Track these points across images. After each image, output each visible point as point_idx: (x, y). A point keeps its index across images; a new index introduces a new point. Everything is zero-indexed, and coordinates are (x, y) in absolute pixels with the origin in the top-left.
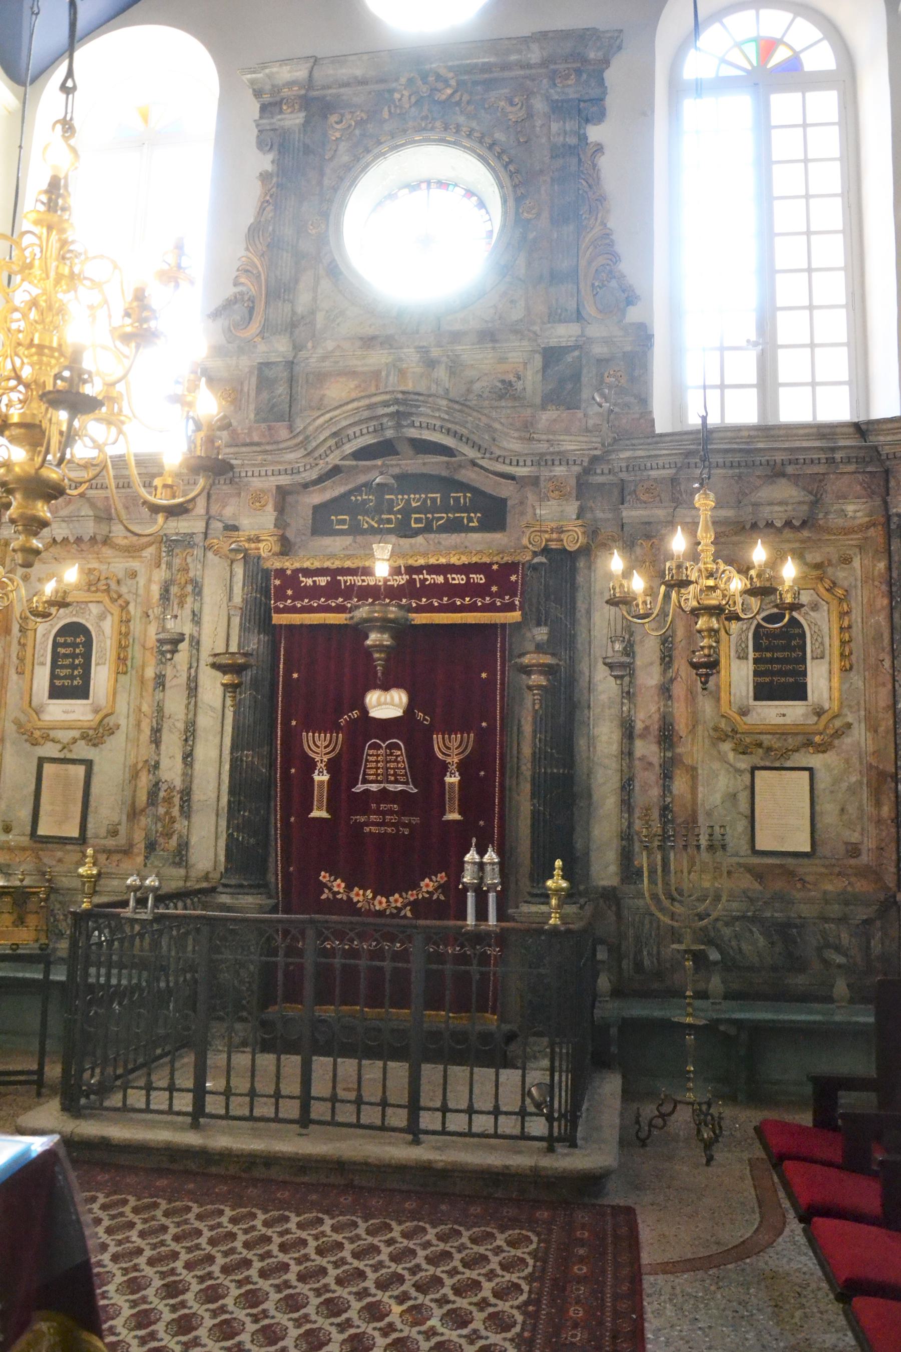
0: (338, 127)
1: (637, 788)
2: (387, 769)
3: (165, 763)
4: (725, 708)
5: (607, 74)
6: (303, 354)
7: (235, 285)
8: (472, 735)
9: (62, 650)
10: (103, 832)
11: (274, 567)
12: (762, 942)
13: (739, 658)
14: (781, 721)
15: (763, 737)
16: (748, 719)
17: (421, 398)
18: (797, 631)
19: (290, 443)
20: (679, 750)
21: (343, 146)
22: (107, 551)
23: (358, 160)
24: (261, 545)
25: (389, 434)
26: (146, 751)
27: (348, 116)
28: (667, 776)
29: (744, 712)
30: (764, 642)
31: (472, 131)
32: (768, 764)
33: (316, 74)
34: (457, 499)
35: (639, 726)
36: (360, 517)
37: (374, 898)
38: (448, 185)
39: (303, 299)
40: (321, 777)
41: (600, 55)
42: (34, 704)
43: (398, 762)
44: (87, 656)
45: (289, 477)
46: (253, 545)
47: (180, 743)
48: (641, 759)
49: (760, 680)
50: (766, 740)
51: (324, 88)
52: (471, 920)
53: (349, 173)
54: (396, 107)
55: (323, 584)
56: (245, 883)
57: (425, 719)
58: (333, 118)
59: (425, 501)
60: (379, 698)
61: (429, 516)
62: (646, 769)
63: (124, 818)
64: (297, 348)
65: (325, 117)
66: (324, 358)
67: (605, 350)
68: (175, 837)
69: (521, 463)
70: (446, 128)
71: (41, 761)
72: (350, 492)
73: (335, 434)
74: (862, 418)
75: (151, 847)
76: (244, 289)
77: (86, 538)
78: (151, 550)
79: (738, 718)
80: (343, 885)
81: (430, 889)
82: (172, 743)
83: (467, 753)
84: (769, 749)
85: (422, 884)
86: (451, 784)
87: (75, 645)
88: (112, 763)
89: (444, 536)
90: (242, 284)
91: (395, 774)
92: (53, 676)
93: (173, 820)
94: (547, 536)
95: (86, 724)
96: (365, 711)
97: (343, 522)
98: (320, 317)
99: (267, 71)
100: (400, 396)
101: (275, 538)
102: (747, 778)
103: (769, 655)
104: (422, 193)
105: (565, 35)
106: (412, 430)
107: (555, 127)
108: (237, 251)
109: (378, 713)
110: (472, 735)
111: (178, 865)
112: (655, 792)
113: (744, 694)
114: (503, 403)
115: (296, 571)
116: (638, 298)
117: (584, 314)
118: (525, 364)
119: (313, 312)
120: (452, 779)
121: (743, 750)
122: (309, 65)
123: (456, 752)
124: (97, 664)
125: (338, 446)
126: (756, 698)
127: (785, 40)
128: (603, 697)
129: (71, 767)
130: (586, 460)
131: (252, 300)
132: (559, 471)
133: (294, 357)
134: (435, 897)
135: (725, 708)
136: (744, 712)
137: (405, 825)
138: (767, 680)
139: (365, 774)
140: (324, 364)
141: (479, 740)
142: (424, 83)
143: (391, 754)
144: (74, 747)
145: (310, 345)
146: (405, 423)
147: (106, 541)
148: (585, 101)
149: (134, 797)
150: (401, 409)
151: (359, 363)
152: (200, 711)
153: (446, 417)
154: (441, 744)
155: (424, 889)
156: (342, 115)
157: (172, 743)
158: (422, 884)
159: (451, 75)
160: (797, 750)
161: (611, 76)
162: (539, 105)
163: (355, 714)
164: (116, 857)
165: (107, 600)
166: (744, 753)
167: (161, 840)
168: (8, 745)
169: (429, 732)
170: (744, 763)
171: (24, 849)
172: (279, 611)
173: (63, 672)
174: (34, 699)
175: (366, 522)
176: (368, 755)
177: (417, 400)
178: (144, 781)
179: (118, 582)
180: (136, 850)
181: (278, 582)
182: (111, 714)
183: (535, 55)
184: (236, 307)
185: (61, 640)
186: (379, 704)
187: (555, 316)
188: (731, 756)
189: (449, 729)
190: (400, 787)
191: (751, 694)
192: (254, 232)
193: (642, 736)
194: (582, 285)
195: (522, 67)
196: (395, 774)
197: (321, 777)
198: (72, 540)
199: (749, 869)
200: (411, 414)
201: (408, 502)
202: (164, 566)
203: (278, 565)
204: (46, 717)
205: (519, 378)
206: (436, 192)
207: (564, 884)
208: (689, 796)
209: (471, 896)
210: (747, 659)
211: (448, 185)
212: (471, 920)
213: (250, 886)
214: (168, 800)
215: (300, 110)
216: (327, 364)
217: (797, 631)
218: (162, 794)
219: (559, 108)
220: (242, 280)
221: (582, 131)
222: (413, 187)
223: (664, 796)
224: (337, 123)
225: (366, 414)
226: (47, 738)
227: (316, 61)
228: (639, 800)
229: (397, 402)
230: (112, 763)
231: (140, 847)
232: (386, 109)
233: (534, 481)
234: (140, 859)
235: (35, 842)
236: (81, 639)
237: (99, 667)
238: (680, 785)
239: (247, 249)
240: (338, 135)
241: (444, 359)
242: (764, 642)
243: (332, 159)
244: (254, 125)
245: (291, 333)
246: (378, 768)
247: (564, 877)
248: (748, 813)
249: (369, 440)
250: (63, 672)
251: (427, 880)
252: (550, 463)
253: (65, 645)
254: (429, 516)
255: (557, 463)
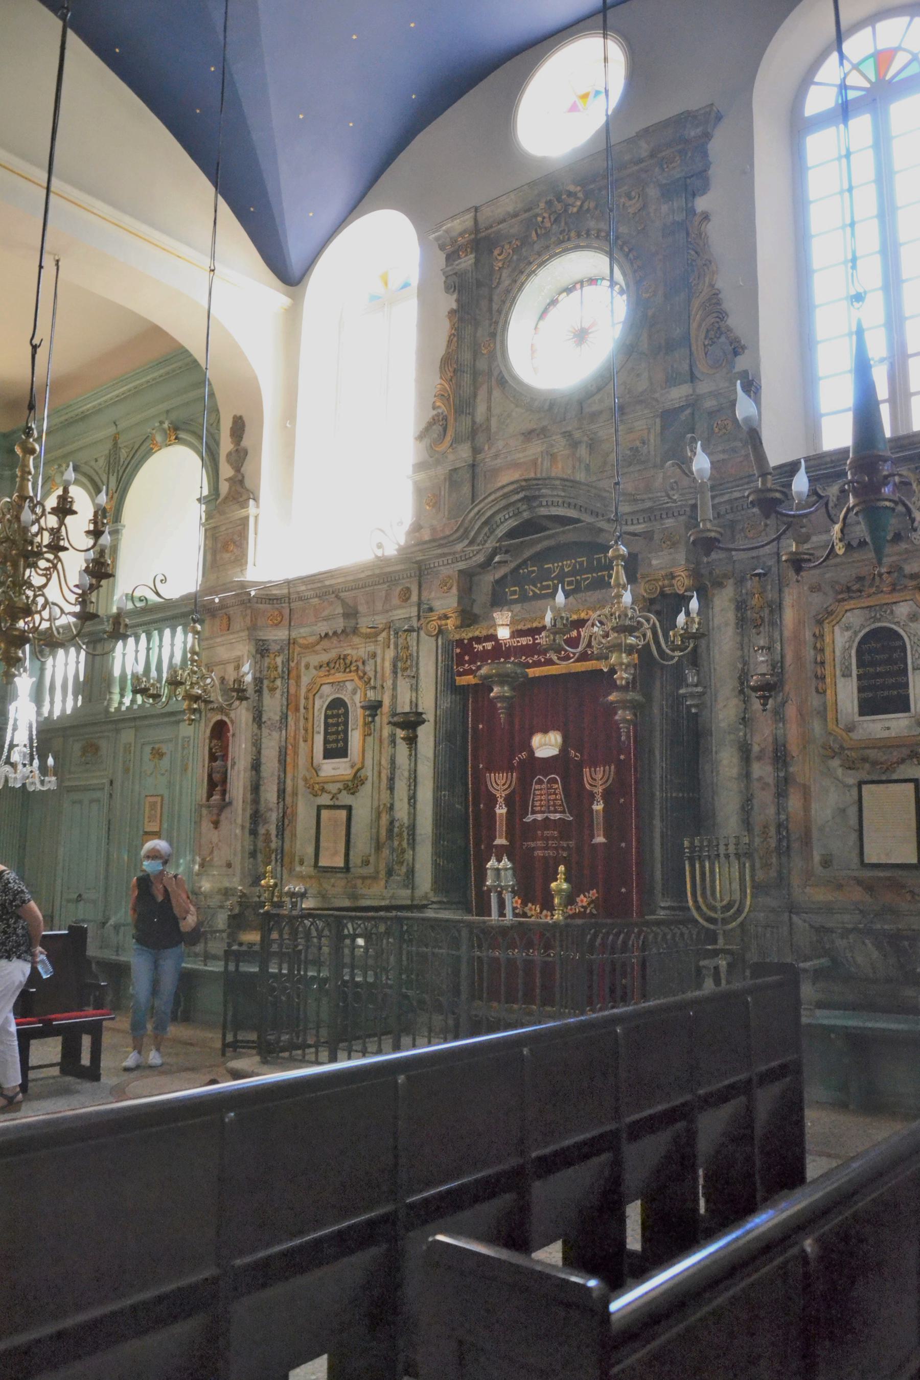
0: (500, 258)
1: (756, 808)
2: (549, 800)
3: (397, 805)
4: (831, 725)
5: (710, 146)
6: (480, 457)
7: (434, 408)
8: (613, 767)
9: (330, 721)
10: (359, 862)
11: (454, 639)
12: (875, 954)
13: (843, 676)
14: (886, 734)
15: (868, 751)
16: (854, 736)
17: (540, 482)
18: (898, 643)
19: (455, 536)
20: (791, 769)
21: (505, 273)
22: (356, 640)
23: (516, 281)
24: (449, 621)
25: (526, 515)
26: (385, 795)
27: (507, 247)
28: (781, 793)
29: (850, 729)
30: (867, 657)
31: (599, 231)
32: (875, 778)
33: (481, 219)
34: (599, 560)
35: (756, 749)
36: (526, 587)
37: (541, 912)
38: (597, 280)
39: (481, 410)
40: (501, 810)
41: (699, 130)
42: (315, 765)
43: (556, 795)
44: (346, 723)
45: (464, 563)
46: (443, 622)
47: (406, 788)
48: (760, 779)
49: (864, 695)
50: (872, 754)
51: (487, 229)
52: (495, 915)
53: (509, 297)
54: (541, 228)
55: (489, 648)
56: (445, 900)
57: (577, 756)
58: (496, 252)
59: (575, 565)
60: (540, 739)
61: (578, 578)
62: (763, 789)
63: (373, 851)
64: (476, 451)
65: (491, 252)
66: (496, 456)
67: (714, 403)
68: (405, 864)
69: (635, 522)
70: (579, 235)
71: (319, 808)
72: (519, 567)
73: (486, 523)
74: (812, 453)
75: (390, 873)
76: (440, 411)
77: (339, 631)
78: (384, 634)
79: (844, 734)
80: (519, 901)
81: (585, 904)
82: (401, 787)
83: (609, 783)
84: (874, 763)
85: (578, 899)
86: (597, 811)
87: (338, 716)
88: (363, 806)
89: (589, 593)
90: (439, 407)
91: (554, 805)
92: (326, 742)
93: (403, 851)
94: (660, 583)
95: (346, 778)
96: (531, 752)
97: (514, 592)
98: (494, 423)
99: (444, 228)
100: (524, 483)
101: (456, 614)
102: (855, 792)
103: (872, 670)
104: (576, 294)
105: (666, 124)
106: (542, 509)
107: (665, 208)
108: (436, 381)
109: (541, 753)
110: (613, 767)
111: (406, 886)
112: (771, 811)
113: (850, 710)
114: (631, 469)
115: (471, 639)
116: (743, 348)
117: (696, 373)
118: (649, 429)
119: (488, 420)
120: (598, 807)
121: (850, 766)
122: (472, 214)
123: (600, 782)
124: (352, 730)
125: (492, 531)
126: (861, 714)
127: (903, 46)
128: (723, 725)
129: (338, 812)
130: (688, 509)
131: (445, 419)
132: (669, 522)
133: (474, 461)
134: (588, 911)
135: (831, 725)
136: (850, 729)
137: (563, 849)
138: (871, 695)
139: (533, 806)
140: (496, 462)
141: (618, 772)
142: (559, 202)
143: (551, 788)
144: (340, 796)
145: (486, 447)
146: (535, 504)
147: (355, 631)
148: (689, 178)
149: (378, 832)
150: (528, 493)
151: (521, 455)
152: (419, 761)
153: (563, 494)
154: (589, 778)
155: (580, 904)
156: (503, 247)
157: (401, 787)
158: (578, 899)
159: (579, 188)
160: (903, 761)
161: (715, 147)
162: (653, 192)
163: (524, 755)
164: (368, 882)
165: (356, 678)
166: (850, 768)
167: (396, 867)
168: (300, 797)
169: (580, 766)
170: (851, 779)
171: (311, 877)
172: (460, 674)
173: (331, 738)
174: (315, 761)
175: (531, 589)
176: (535, 790)
177: (537, 485)
178: (385, 819)
179: (364, 663)
180: (381, 876)
181: (458, 651)
182: (362, 768)
183: (644, 148)
184: (434, 427)
185: (329, 712)
186: (541, 745)
187: (672, 380)
188: (840, 771)
189: (594, 764)
190: (558, 816)
191: (856, 709)
192: (446, 361)
193: (759, 758)
194: (694, 348)
195: (636, 164)
196: (554, 805)
197: (501, 810)
198: (331, 634)
199: (859, 882)
200: (539, 496)
201: (562, 568)
202: (392, 646)
203: (457, 637)
204: (322, 774)
205: (644, 443)
206: (588, 289)
207: (565, 886)
208: (802, 813)
209: (493, 896)
210: (851, 676)
211: (597, 280)
212: (495, 915)
213: (448, 903)
214: (400, 835)
215: (471, 253)
216: (499, 461)
217: (898, 643)
218: (396, 830)
219: (667, 193)
220: (438, 404)
221: (690, 205)
222: (568, 290)
223: (779, 813)
224: (499, 255)
225: (503, 503)
226: (323, 790)
227: (476, 209)
228: (758, 819)
229: (523, 489)
230: (363, 806)
231: (382, 874)
232: (534, 233)
233: (648, 536)
234: (382, 883)
235: (319, 871)
236: (342, 711)
237: (354, 732)
238: (794, 803)
239: (441, 378)
240: (500, 264)
241: (585, 438)
242: (867, 657)
243: (497, 286)
244: (441, 273)
245: (473, 439)
246: (541, 800)
247: (566, 880)
248: (857, 827)
249: (512, 523)
250: (331, 738)
251: (582, 896)
252: (658, 517)
253: (333, 716)
254: (578, 578)
255: (664, 516)
